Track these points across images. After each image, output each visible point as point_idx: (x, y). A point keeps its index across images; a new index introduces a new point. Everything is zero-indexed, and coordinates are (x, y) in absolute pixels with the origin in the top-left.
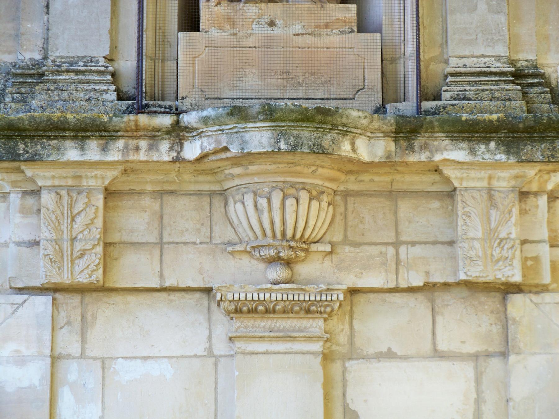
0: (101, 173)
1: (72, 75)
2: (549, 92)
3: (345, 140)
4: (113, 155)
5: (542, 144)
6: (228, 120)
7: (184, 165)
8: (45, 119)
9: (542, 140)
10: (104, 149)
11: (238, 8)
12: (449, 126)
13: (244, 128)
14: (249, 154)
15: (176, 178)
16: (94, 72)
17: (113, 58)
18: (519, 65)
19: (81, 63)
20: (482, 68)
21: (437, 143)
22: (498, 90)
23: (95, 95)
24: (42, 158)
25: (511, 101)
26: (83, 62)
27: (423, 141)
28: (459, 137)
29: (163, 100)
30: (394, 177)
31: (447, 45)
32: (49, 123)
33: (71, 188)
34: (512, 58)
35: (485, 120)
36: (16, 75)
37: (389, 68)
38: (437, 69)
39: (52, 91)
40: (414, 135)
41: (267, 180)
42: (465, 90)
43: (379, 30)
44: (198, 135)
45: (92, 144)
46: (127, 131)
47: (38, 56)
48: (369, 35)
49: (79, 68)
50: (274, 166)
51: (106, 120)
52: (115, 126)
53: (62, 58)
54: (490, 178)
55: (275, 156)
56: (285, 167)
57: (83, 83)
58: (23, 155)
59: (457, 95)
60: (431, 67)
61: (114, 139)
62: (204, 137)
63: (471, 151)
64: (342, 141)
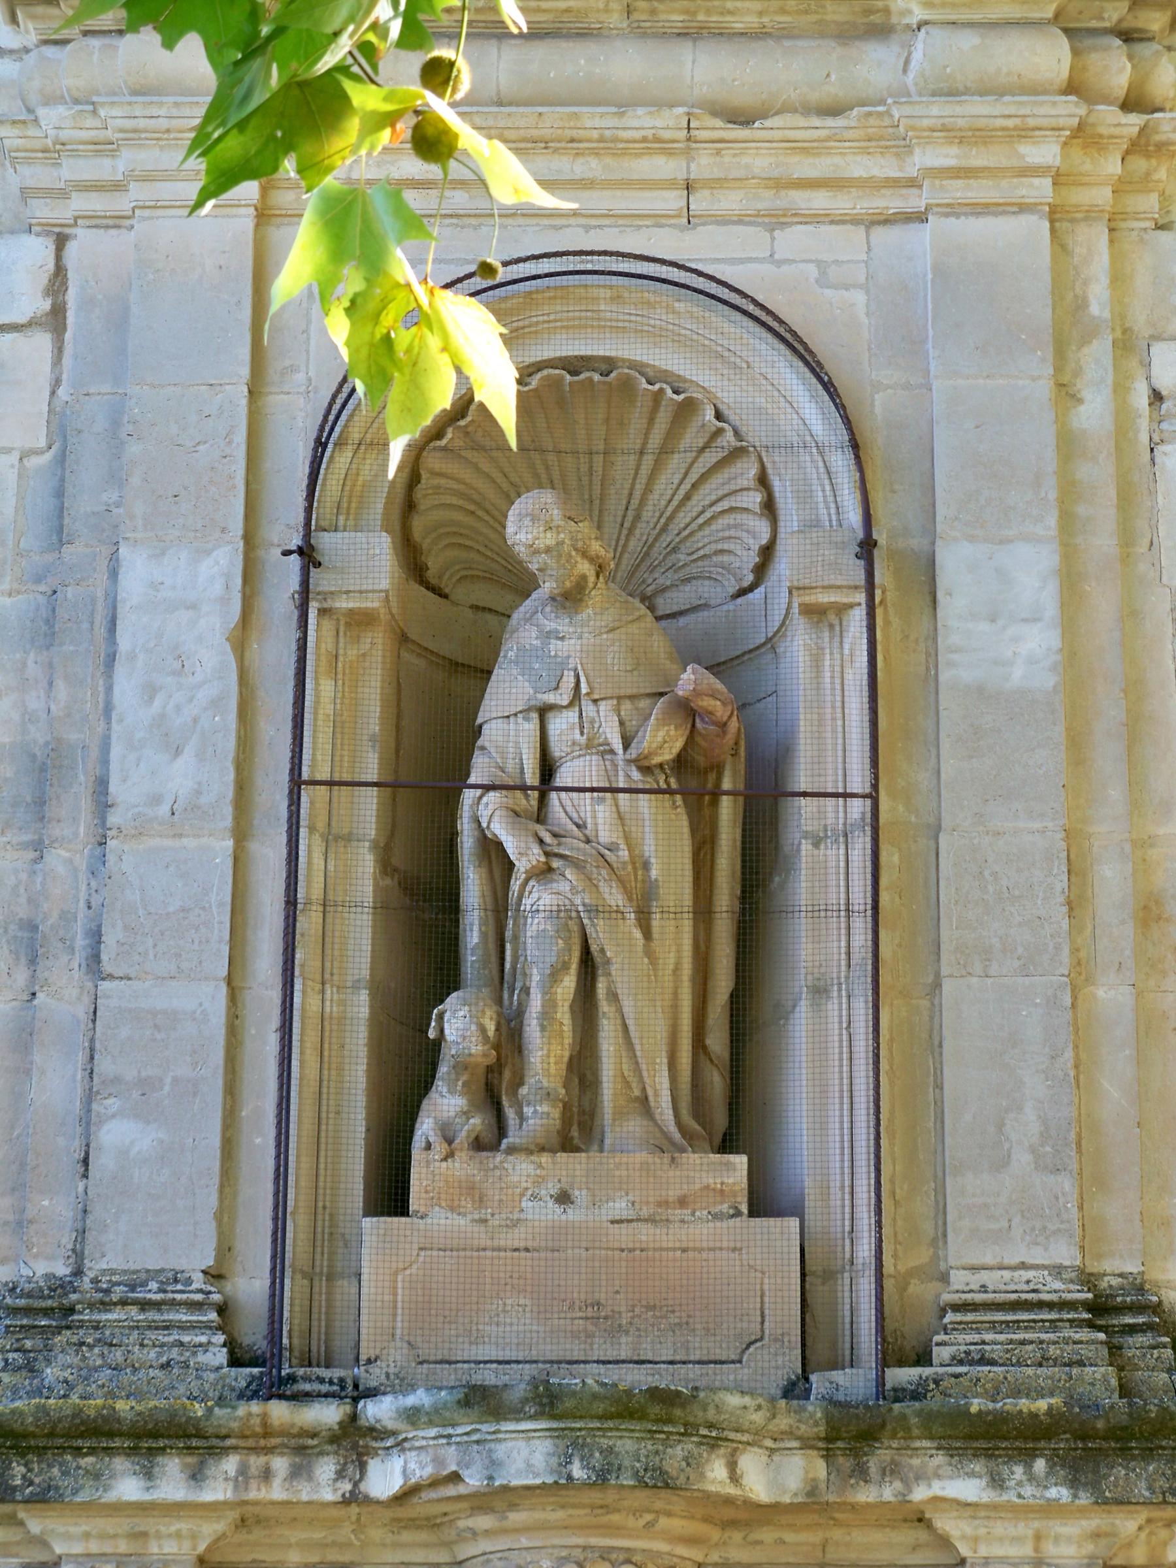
0: (190, 1526)
1: (133, 1311)
2: (1169, 1346)
3: (714, 1456)
4: (215, 1489)
5: (1148, 1464)
6: (457, 1416)
7: (370, 1509)
8: (69, 1412)
9: (1148, 1454)
10: (196, 1476)
11: (491, 1166)
12: (943, 1425)
13: (494, 1433)
14: (505, 1489)
15: (353, 1537)
16: (180, 1304)
17: (223, 1272)
18: (1103, 1284)
19: (154, 1285)
20: (1022, 1292)
21: (919, 1461)
22: (1055, 1343)
23: (182, 1355)
24: (61, 1495)
25: (1085, 1365)
26: (157, 1282)
27: (888, 1458)
28: (966, 1449)
29: (327, 1367)
30: (828, 1535)
31: (946, 1242)
32: (78, 1421)
33: (124, 1559)
34: (1087, 1271)
35: (1021, 1411)
36: (14, 1311)
37: (818, 1292)
38: (923, 1291)
39: (89, 1345)
40: (868, 1445)
41: (548, 1543)
42: (983, 1343)
43: (797, 1210)
44: (398, 1445)
45: (171, 1465)
46: (246, 1437)
47: (62, 1270)
48: (772, 1221)
49: (149, 1296)
50: (561, 1514)
51: (200, 1414)
52: (220, 1426)
53: (111, 1275)
54: (1038, 1538)
55: (563, 1492)
56: (586, 1515)
57: (157, 1328)
58: (22, 1488)
59: (965, 1352)
60: (911, 1289)
61: (216, 1454)
62: (410, 1449)
63: (993, 1480)
64: (708, 1461)
